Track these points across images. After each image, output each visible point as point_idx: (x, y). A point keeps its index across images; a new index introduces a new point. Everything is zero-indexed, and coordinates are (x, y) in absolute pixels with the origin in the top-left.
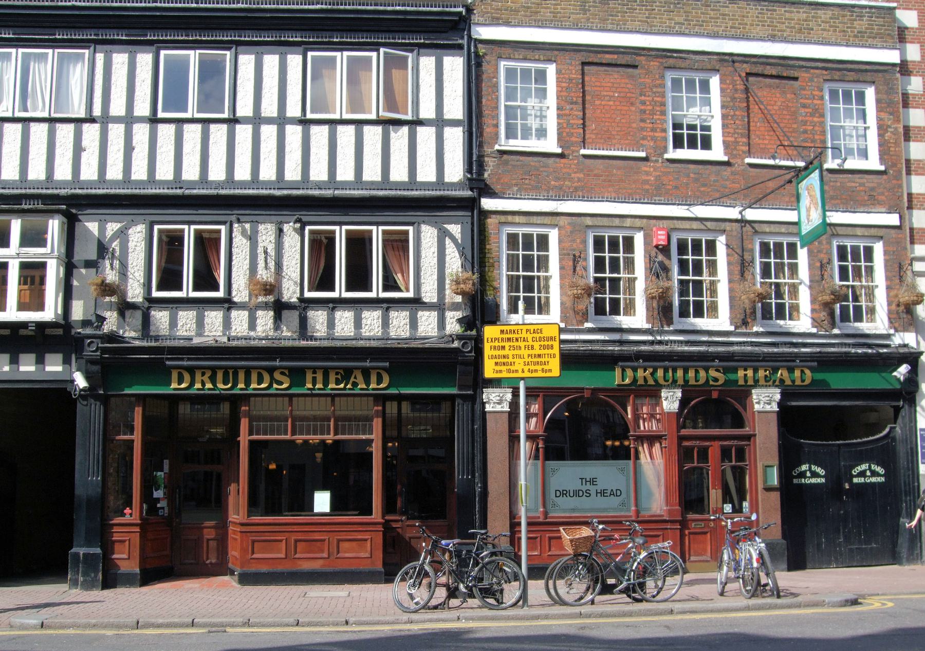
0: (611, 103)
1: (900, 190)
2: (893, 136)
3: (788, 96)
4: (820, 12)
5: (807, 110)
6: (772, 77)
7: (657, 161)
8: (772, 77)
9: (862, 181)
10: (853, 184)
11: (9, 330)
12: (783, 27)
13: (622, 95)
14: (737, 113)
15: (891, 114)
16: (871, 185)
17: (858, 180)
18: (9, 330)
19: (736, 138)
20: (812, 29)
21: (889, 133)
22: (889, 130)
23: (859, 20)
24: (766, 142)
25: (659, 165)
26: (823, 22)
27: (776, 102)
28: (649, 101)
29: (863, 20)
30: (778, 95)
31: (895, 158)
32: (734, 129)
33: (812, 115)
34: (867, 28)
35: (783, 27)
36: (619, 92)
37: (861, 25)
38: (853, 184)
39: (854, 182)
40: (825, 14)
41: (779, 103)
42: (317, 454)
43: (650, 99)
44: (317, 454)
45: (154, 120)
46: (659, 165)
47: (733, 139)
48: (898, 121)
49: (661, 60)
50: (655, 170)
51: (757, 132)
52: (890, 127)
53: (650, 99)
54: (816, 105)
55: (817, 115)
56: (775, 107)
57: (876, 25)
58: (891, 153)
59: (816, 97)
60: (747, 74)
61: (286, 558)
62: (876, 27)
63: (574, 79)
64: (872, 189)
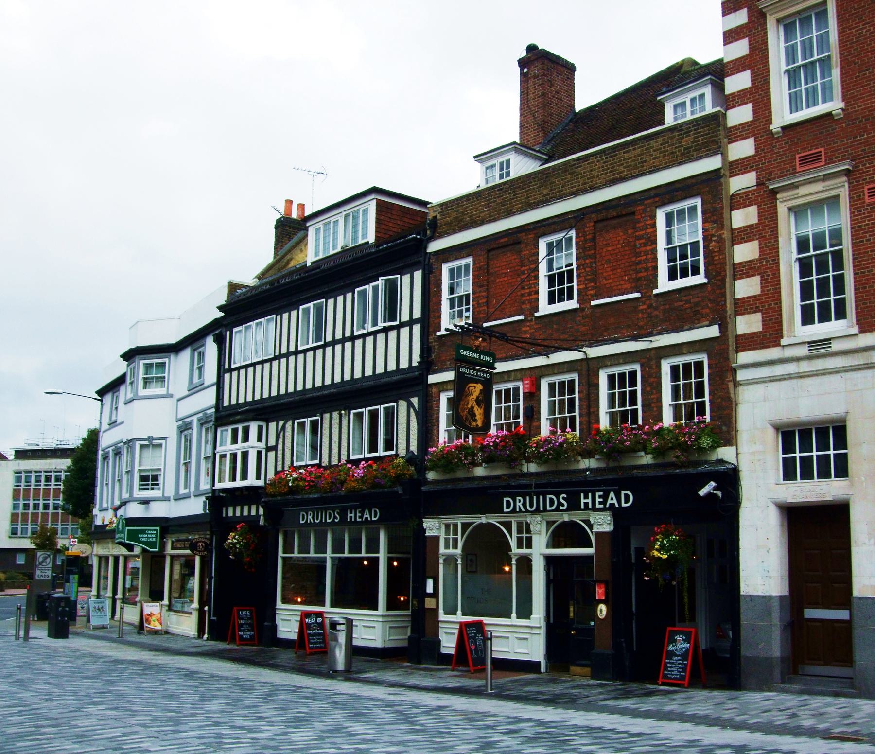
0: (506, 279)
1: (723, 299)
2: (717, 245)
3: (629, 231)
4: (652, 143)
5: (641, 241)
6: (614, 218)
7: (531, 320)
8: (614, 218)
9: (687, 298)
10: (681, 303)
11: (756, 280)
12: (621, 168)
13: (513, 269)
14: (587, 261)
15: (715, 222)
16: (696, 300)
17: (684, 298)
18: (756, 280)
19: (586, 285)
20: (645, 161)
21: (713, 243)
22: (713, 239)
23: (686, 137)
24: (611, 281)
25: (533, 323)
26: (654, 151)
27: (619, 240)
28: (527, 270)
29: (689, 136)
30: (621, 234)
31: (719, 266)
32: (585, 276)
33: (645, 245)
34: (693, 142)
35: (621, 168)
36: (510, 268)
37: (687, 141)
38: (681, 303)
39: (681, 301)
40: (656, 142)
41: (622, 242)
42: (432, 527)
43: (528, 267)
44: (432, 527)
45: (353, 339)
46: (533, 323)
47: (584, 286)
48: (722, 226)
49: (535, 232)
50: (530, 329)
51: (604, 274)
52: (713, 236)
53: (528, 267)
54: (649, 233)
55: (650, 243)
56: (619, 246)
57: (701, 136)
58: (715, 262)
59: (649, 227)
60: (595, 222)
61: (476, 555)
62: (700, 138)
63: (482, 266)
64: (696, 304)
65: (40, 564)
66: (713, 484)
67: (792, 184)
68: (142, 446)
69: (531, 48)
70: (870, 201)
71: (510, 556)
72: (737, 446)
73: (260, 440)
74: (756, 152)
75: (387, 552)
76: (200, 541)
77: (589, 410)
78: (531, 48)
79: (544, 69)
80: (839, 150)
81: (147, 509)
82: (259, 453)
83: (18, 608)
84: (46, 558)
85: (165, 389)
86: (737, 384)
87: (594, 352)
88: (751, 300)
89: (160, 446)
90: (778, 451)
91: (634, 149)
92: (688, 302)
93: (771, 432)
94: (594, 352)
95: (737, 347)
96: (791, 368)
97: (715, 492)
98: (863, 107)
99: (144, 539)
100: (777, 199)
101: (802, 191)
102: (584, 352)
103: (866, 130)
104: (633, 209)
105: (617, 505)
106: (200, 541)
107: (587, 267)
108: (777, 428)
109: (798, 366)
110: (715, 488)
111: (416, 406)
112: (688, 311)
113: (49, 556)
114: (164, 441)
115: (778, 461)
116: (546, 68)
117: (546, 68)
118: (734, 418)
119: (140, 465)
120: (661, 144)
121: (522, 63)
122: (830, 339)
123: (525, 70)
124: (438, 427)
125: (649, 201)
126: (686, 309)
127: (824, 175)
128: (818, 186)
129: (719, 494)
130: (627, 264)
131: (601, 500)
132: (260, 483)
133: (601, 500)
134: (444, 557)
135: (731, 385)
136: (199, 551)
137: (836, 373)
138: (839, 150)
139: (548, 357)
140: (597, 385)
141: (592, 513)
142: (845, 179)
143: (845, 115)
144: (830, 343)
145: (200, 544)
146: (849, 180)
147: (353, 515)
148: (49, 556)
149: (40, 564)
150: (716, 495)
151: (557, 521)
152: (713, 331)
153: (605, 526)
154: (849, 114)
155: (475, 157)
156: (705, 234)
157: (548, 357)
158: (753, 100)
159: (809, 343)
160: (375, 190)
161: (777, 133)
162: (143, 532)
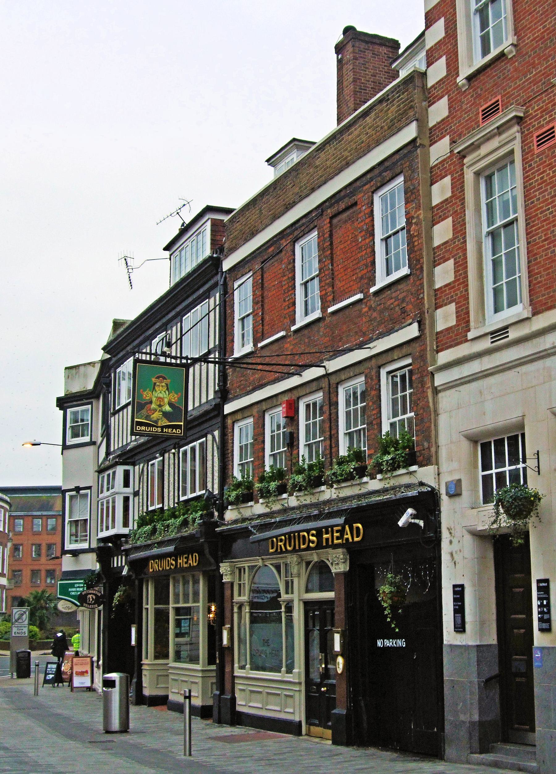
65: (16, 621)
66: (410, 511)
67: (472, 144)
68: (71, 497)
69: (349, 30)
70: (539, 150)
71: (279, 602)
72: (437, 464)
73: (126, 484)
74: (450, 112)
75: (207, 601)
76: (90, 594)
77: (331, 433)
78: (349, 30)
79: (354, 52)
80: (513, 94)
81: (77, 562)
82: (126, 500)
83: (36, 665)
84: (22, 615)
85: (89, 437)
86: (436, 391)
87: (334, 365)
88: (447, 288)
89: (86, 495)
90: (476, 467)
91: (355, 129)
92: (397, 299)
93: (466, 445)
94: (334, 365)
95: (437, 347)
96: (474, 367)
97: (413, 521)
98: (531, 38)
99: (73, 593)
100: (464, 165)
101: (484, 150)
102: (324, 367)
103: (534, 65)
104: (355, 198)
105: (351, 540)
106: (90, 594)
107: (327, 270)
108: (473, 440)
109: (481, 363)
110: (414, 517)
111: (217, 441)
112: (397, 308)
113: (25, 612)
114: (89, 491)
115: (476, 481)
116: (357, 51)
117: (357, 51)
118: (433, 432)
119: (70, 517)
120: (374, 119)
121: (339, 49)
122: (506, 327)
123: (340, 57)
124: (233, 462)
125: (367, 187)
126: (394, 307)
127: (498, 128)
128: (495, 143)
129: (421, 523)
130: (355, 262)
131: (338, 534)
132: (126, 531)
133: (338, 534)
134: (285, 603)
135: (430, 393)
136: (90, 604)
137: (510, 368)
138: (513, 94)
139: (301, 375)
140: (337, 403)
141: (330, 550)
142: (516, 128)
143: (517, 51)
144: (508, 332)
145: (90, 596)
146: (521, 129)
147: (181, 561)
148: (25, 612)
149: (16, 621)
150: (417, 525)
151: (311, 562)
152: (412, 331)
153: (340, 566)
154: (520, 49)
155: (268, 161)
156: (408, 217)
157: (301, 375)
158: (446, 52)
159: (492, 333)
160: (209, 209)
161: (463, 85)
162: (72, 585)
